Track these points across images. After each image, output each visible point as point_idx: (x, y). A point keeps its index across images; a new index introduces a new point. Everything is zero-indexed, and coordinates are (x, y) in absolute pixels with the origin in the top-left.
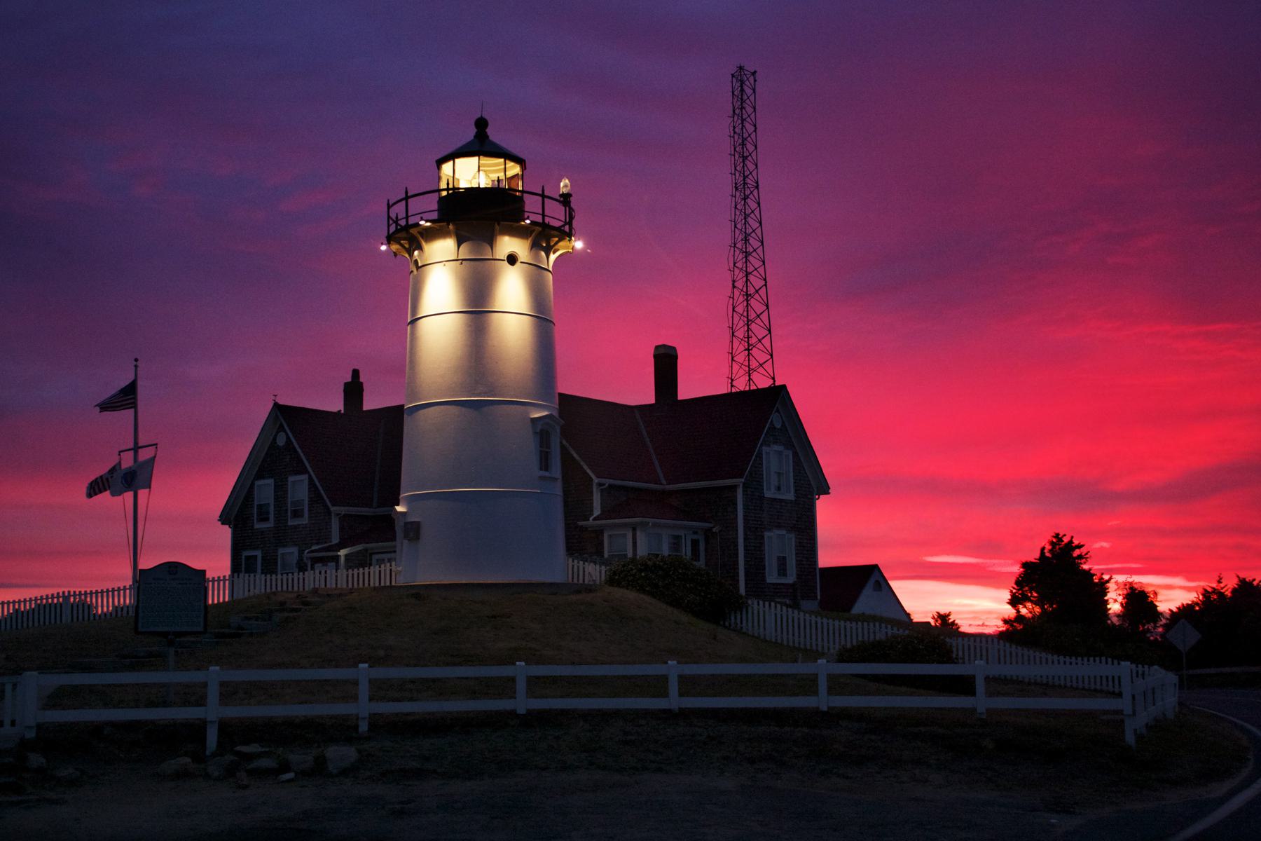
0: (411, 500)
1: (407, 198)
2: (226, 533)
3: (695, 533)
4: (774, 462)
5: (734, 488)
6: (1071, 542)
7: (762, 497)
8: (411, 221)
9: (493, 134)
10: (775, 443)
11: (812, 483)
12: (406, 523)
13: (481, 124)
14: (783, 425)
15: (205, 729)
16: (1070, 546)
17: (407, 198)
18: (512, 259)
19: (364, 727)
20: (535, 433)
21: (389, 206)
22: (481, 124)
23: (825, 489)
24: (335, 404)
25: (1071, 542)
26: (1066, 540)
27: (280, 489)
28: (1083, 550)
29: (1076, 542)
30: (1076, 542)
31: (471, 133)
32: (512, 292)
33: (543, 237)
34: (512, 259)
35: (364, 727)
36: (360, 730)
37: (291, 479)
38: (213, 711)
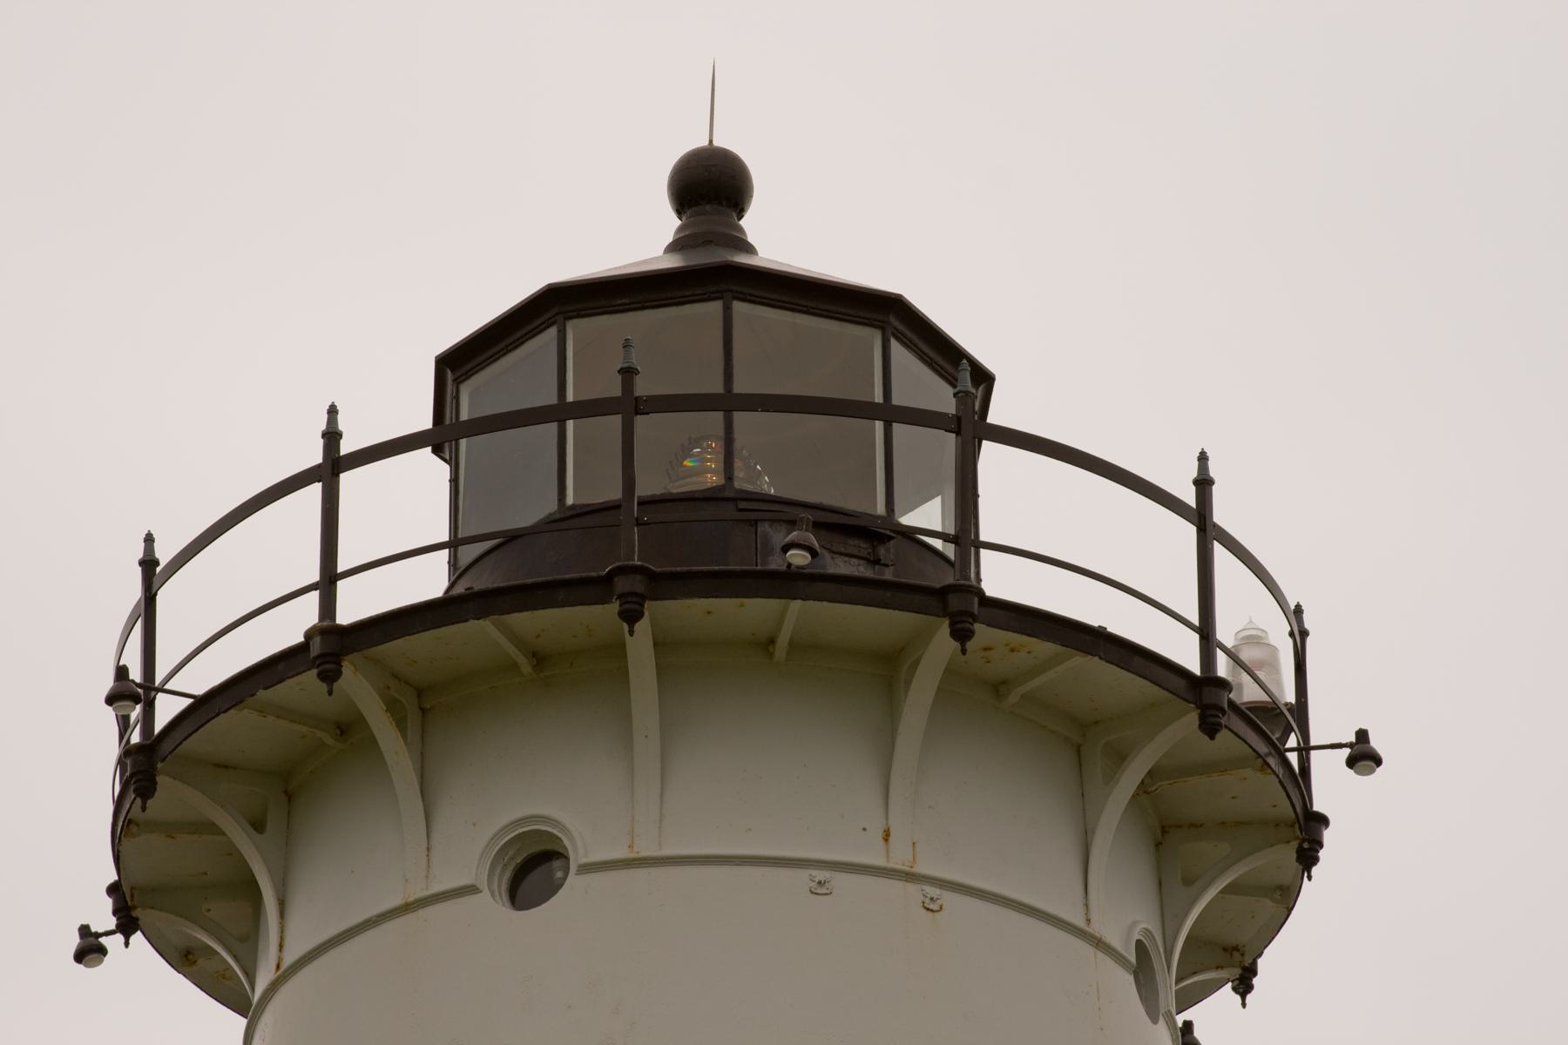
1: (333, 466)
17: (333, 466)
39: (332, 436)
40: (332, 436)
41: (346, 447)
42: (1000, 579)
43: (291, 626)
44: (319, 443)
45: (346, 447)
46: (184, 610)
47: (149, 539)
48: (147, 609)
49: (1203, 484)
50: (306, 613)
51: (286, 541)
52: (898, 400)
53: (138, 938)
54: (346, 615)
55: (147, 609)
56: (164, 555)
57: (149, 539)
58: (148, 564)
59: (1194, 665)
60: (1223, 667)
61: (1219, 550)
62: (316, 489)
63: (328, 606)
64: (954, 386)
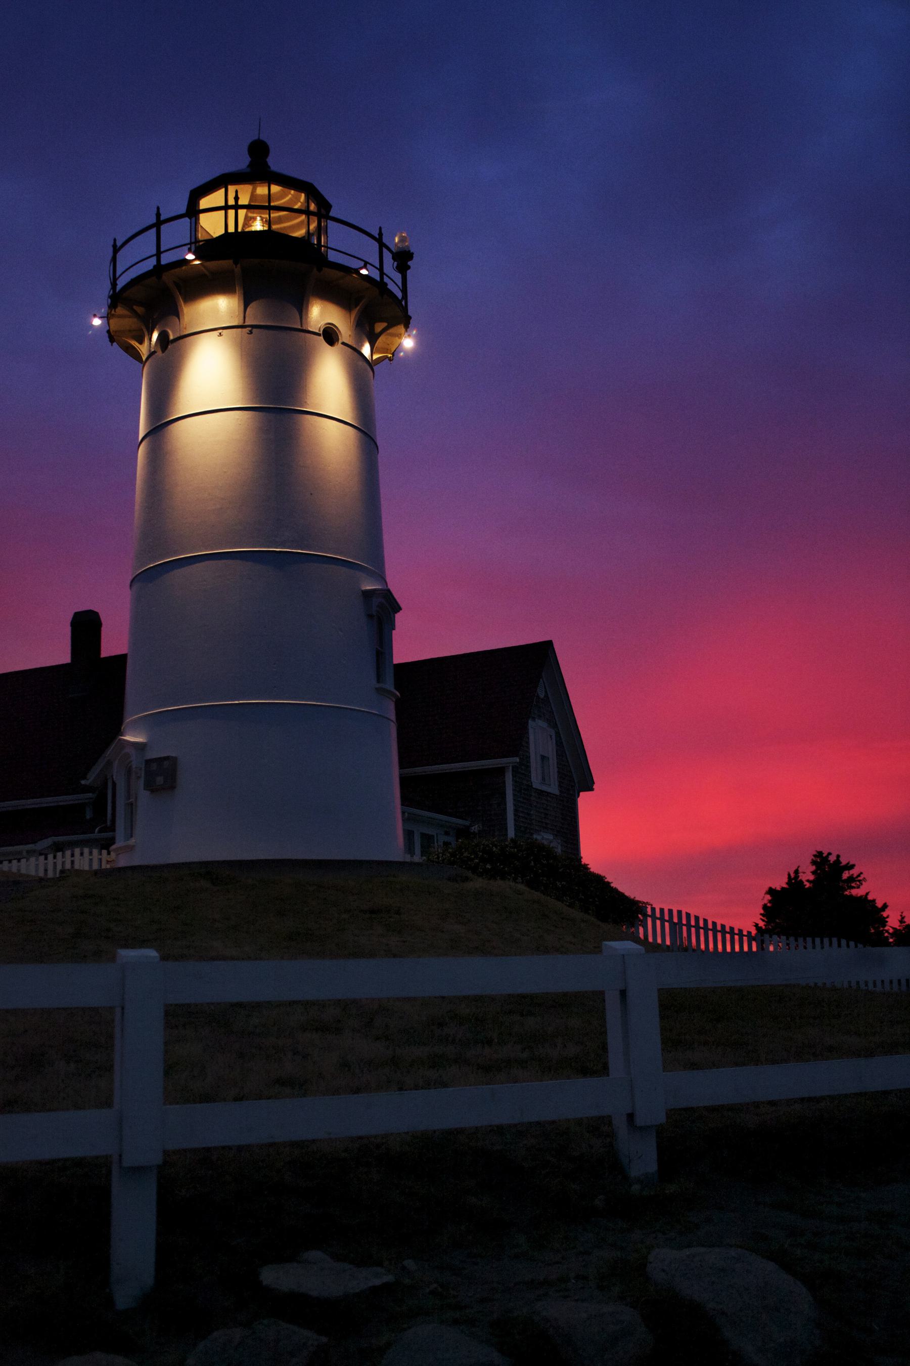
0: (155, 722)
1: (158, 224)
2: (410, 313)
3: (447, 833)
4: (539, 739)
5: (501, 771)
6: (838, 861)
7: (530, 786)
8: (166, 259)
9: (275, 163)
10: (540, 717)
11: (577, 776)
12: (148, 762)
13: (259, 150)
14: (546, 696)
15: (105, 1194)
16: (838, 867)
17: (158, 224)
18: (330, 335)
19: (642, 1159)
20: (370, 616)
21: (116, 250)
22: (259, 150)
23: (588, 785)
25: (838, 861)
26: (832, 859)
28: (854, 872)
29: (844, 861)
30: (844, 861)
31: (242, 162)
32: (329, 384)
33: (376, 309)
34: (330, 335)
35: (642, 1159)
36: (635, 1171)
38: (139, 1122)
39: (158, 215)
40: (158, 215)
41: (162, 218)
42: (332, 256)
43: (151, 263)
44: (111, 249)
45: (162, 218)
46: (125, 258)
47: (115, 240)
48: (114, 260)
49: (381, 234)
50: (153, 262)
51: (146, 245)
52: (154, 252)
53: (115, 344)
54: (163, 262)
55: (114, 260)
56: (119, 244)
57: (115, 240)
58: (114, 246)
59: (378, 279)
60: (386, 279)
61: (385, 250)
62: (154, 229)
63: (159, 260)
64: (378, 681)
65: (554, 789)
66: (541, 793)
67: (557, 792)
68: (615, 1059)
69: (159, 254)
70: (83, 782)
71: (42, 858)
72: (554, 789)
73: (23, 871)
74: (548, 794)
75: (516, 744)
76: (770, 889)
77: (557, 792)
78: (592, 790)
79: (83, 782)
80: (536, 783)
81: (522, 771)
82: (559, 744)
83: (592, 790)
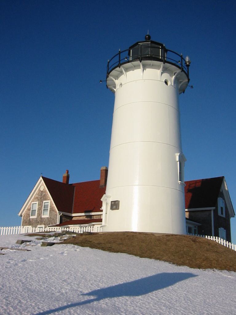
3: (195, 227)
4: (220, 203)
5: (210, 210)
24: (61, 180)
27: (40, 204)
37: (44, 202)
50: (118, 63)
65: (224, 216)
66: (221, 217)
67: (225, 217)
68: (103, 220)
69: (120, 61)
70: (101, 209)
71: (75, 232)
72: (224, 216)
73: (70, 231)
74: (223, 217)
75: (215, 204)
76: (102, 211)
77: (225, 217)
78: (111, 209)
79: (101, 209)
80: (219, 213)
81: (216, 211)
82: (226, 204)
83: (111, 209)
